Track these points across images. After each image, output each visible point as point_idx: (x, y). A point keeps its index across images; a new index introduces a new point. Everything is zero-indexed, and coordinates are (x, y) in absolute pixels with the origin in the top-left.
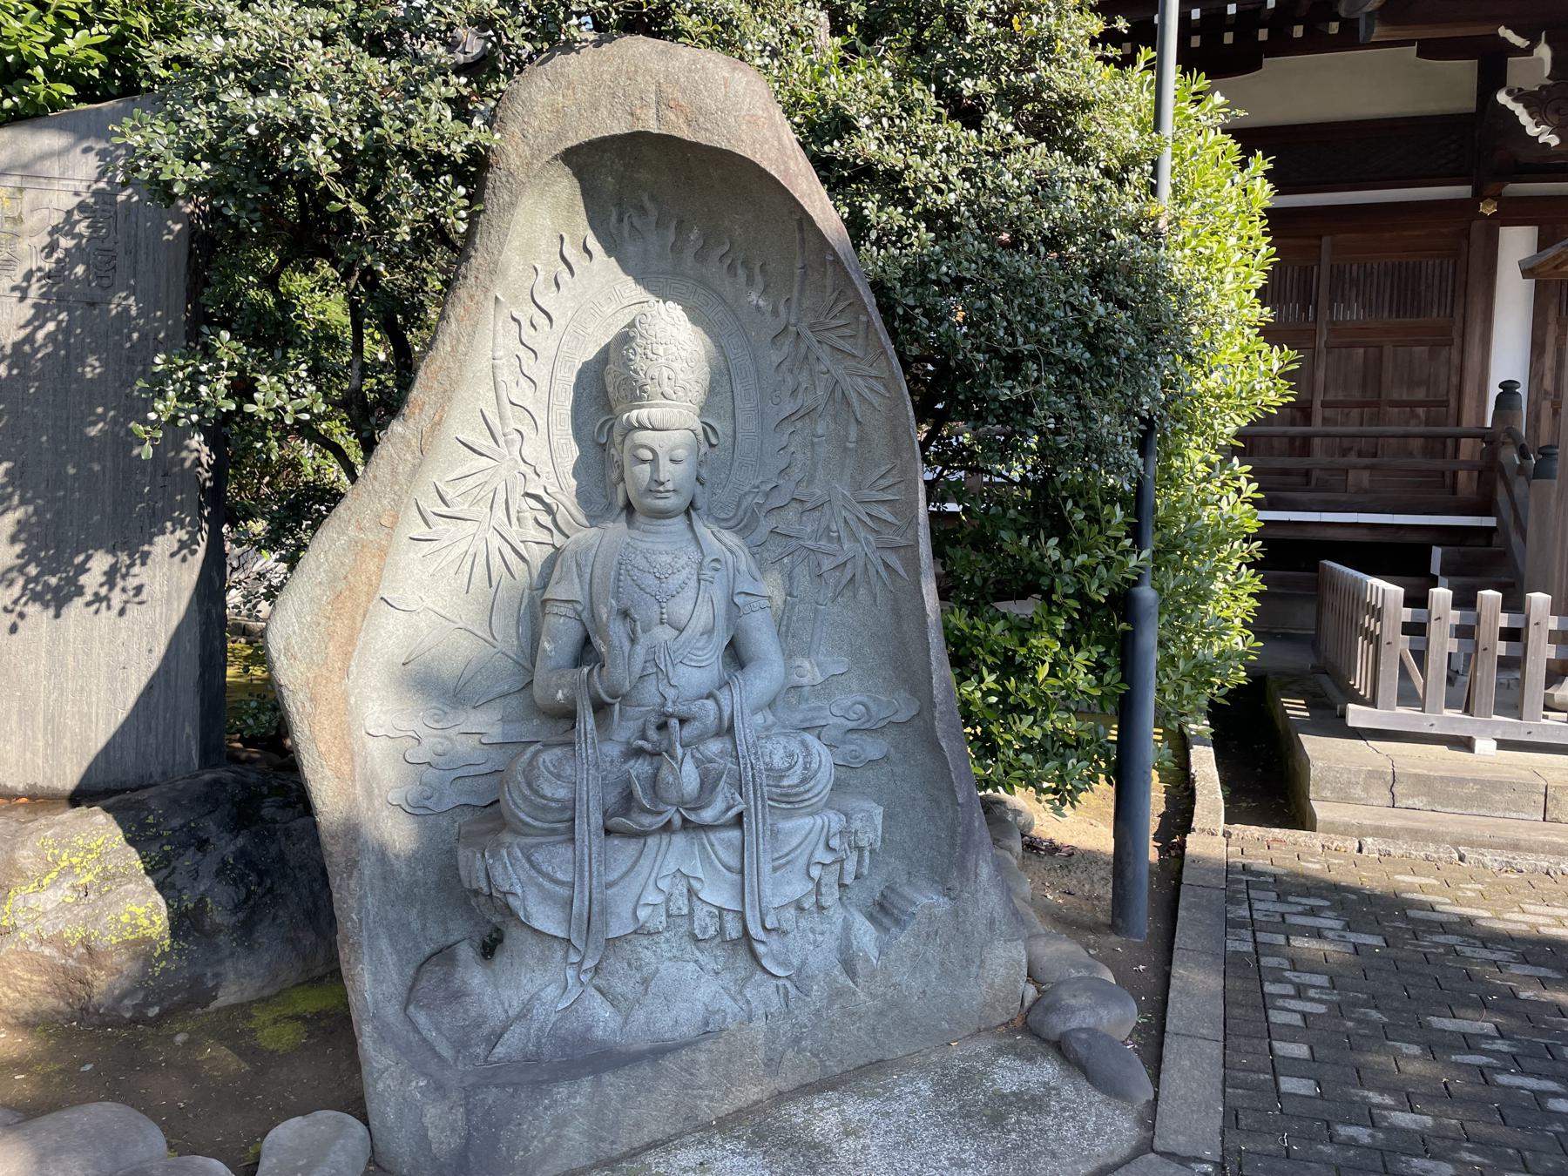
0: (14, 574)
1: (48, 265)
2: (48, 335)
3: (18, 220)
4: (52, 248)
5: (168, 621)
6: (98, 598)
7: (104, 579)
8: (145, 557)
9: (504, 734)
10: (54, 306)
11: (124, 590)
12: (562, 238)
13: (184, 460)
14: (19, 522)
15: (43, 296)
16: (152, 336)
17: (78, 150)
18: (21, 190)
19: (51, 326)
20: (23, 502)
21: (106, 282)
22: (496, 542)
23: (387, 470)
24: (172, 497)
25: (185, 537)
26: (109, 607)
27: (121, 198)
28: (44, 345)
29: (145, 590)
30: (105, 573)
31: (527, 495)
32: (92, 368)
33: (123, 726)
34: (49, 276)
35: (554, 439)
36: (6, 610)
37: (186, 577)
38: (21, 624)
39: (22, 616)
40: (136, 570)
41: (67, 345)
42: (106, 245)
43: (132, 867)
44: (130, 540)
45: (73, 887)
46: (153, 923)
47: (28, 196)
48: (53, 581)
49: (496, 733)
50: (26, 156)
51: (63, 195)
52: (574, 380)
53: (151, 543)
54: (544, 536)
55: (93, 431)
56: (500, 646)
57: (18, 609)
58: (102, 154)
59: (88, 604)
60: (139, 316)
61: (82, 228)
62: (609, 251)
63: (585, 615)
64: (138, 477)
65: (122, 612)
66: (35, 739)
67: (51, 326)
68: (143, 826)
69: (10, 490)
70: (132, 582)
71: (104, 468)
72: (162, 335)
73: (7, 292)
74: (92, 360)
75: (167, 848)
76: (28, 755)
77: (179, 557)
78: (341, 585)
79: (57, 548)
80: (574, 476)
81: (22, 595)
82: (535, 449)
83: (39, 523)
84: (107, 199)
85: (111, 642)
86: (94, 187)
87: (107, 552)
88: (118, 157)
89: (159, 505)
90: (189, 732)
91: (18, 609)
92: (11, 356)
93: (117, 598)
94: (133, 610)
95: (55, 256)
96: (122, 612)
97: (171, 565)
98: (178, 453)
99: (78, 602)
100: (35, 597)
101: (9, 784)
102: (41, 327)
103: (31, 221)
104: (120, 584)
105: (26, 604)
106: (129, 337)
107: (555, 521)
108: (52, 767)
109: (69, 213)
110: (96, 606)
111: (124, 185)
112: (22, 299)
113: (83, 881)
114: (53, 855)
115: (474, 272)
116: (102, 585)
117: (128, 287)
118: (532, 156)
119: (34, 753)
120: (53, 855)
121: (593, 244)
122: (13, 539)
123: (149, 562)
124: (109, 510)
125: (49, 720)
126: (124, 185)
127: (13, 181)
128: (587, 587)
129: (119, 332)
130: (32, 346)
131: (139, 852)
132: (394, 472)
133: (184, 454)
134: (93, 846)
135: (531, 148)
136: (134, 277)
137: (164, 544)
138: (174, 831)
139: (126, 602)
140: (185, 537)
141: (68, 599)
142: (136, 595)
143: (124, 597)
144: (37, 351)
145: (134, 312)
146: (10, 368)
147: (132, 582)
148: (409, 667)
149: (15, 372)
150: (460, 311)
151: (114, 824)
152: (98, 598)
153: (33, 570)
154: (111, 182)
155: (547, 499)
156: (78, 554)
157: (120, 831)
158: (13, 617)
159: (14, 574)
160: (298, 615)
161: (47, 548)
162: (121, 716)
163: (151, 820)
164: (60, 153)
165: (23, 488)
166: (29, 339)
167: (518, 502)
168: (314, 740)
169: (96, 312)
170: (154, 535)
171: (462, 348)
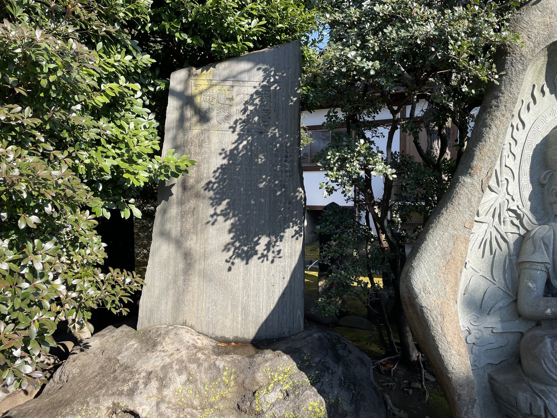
0: (230, 246)
1: (244, 117)
2: (243, 146)
3: (232, 99)
4: (245, 110)
5: (291, 265)
6: (263, 256)
7: (265, 247)
8: (282, 238)
9: (503, 328)
10: (246, 134)
11: (273, 252)
12: (534, 86)
13: (297, 196)
14: (232, 224)
15: (241, 130)
16: (284, 145)
17: (256, 69)
18: (232, 87)
19: (245, 143)
20: (234, 216)
21: (266, 123)
22: (495, 233)
23: (465, 200)
24: (292, 212)
25: (298, 229)
26: (267, 260)
27: (272, 88)
28: (242, 151)
29: (282, 252)
30: (266, 245)
31: (509, 210)
32: (261, 159)
33: (273, 311)
34: (244, 122)
35: (521, 183)
36: (227, 261)
37: (298, 246)
38: (233, 267)
39: (233, 264)
40: (278, 243)
41: (251, 150)
42: (266, 108)
43: (305, 382)
44: (276, 231)
45: (281, 390)
46: (321, 410)
47: (236, 89)
48: (246, 249)
49: (499, 328)
50: (234, 73)
51: (249, 88)
52: (531, 153)
53: (284, 232)
54: (515, 230)
55: (261, 186)
56: (498, 285)
57: (231, 261)
58: (265, 70)
59: (259, 258)
60: (279, 137)
61: (257, 101)
62: (551, 92)
63: (550, 270)
64: (279, 204)
65: (272, 262)
66: (238, 317)
67: (245, 143)
68: (303, 361)
69: (228, 211)
70: (276, 249)
71: (265, 200)
72: (289, 144)
73: (228, 129)
74: (261, 156)
75: (317, 372)
76: (235, 324)
77: (295, 238)
78: (449, 257)
79: (247, 235)
80: (529, 200)
81: (233, 255)
82: (513, 188)
83: (240, 225)
84: (267, 89)
85: (268, 274)
86: (262, 84)
87: (267, 236)
88: (271, 71)
89: (287, 216)
90: (300, 313)
91: (231, 261)
92: (229, 155)
93: (271, 255)
94: (276, 260)
95: (246, 113)
96: (272, 262)
97: (292, 241)
98: (295, 193)
99: (255, 257)
100: (239, 256)
101: (227, 336)
102: (241, 143)
103: (237, 99)
104: (272, 249)
105: (234, 259)
106: (276, 146)
107: (521, 223)
108: (244, 329)
109: (252, 95)
110: (262, 259)
111: (274, 82)
112: (233, 132)
113: (285, 388)
114: (271, 375)
115: (504, 104)
116: (264, 250)
117: (275, 125)
118: (535, 47)
119: (237, 323)
120: (271, 375)
121: (546, 89)
122: (230, 231)
123: (283, 240)
124: (267, 218)
125: (244, 309)
126: (274, 82)
127: (229, 83)
128: (551, 256)
129: (272, 144)
130: (237, 151)
131: (307, 375)
132: (469, 201)
133: (297, 194)
134: (286, 371)
135: (534, 43)
136: (278, 121)
137: (289, 232)
138: (317, 364)
139: (274, 257)
140: (298, 229)
141: (251, 256)
142: (278, 254)
143: (273, 255)
144: (240, 153)
145: (277, 135)
146: (229, 160)
147: (276, 249)
148: (465, 295)
149: (231, 162)
150: (497, 122)
151: (292, 360)
152: (263, 256)
153: (237, 244)
154: (268, 82)
155: (519, 212)
156: (255, 237)
157: (295, 363)
158: (229, 264)
159: (230, 246)
160: (429, 272)
161: (243, 235)
162: (272, 307)
163: (305, 358)
164: (249, 71)
165: (234, 210)
166: (236, 148)
167: (508, 216)
168: (444, 335)
169: (263, 136)
170: (285, 229)
171: (500, 140)
